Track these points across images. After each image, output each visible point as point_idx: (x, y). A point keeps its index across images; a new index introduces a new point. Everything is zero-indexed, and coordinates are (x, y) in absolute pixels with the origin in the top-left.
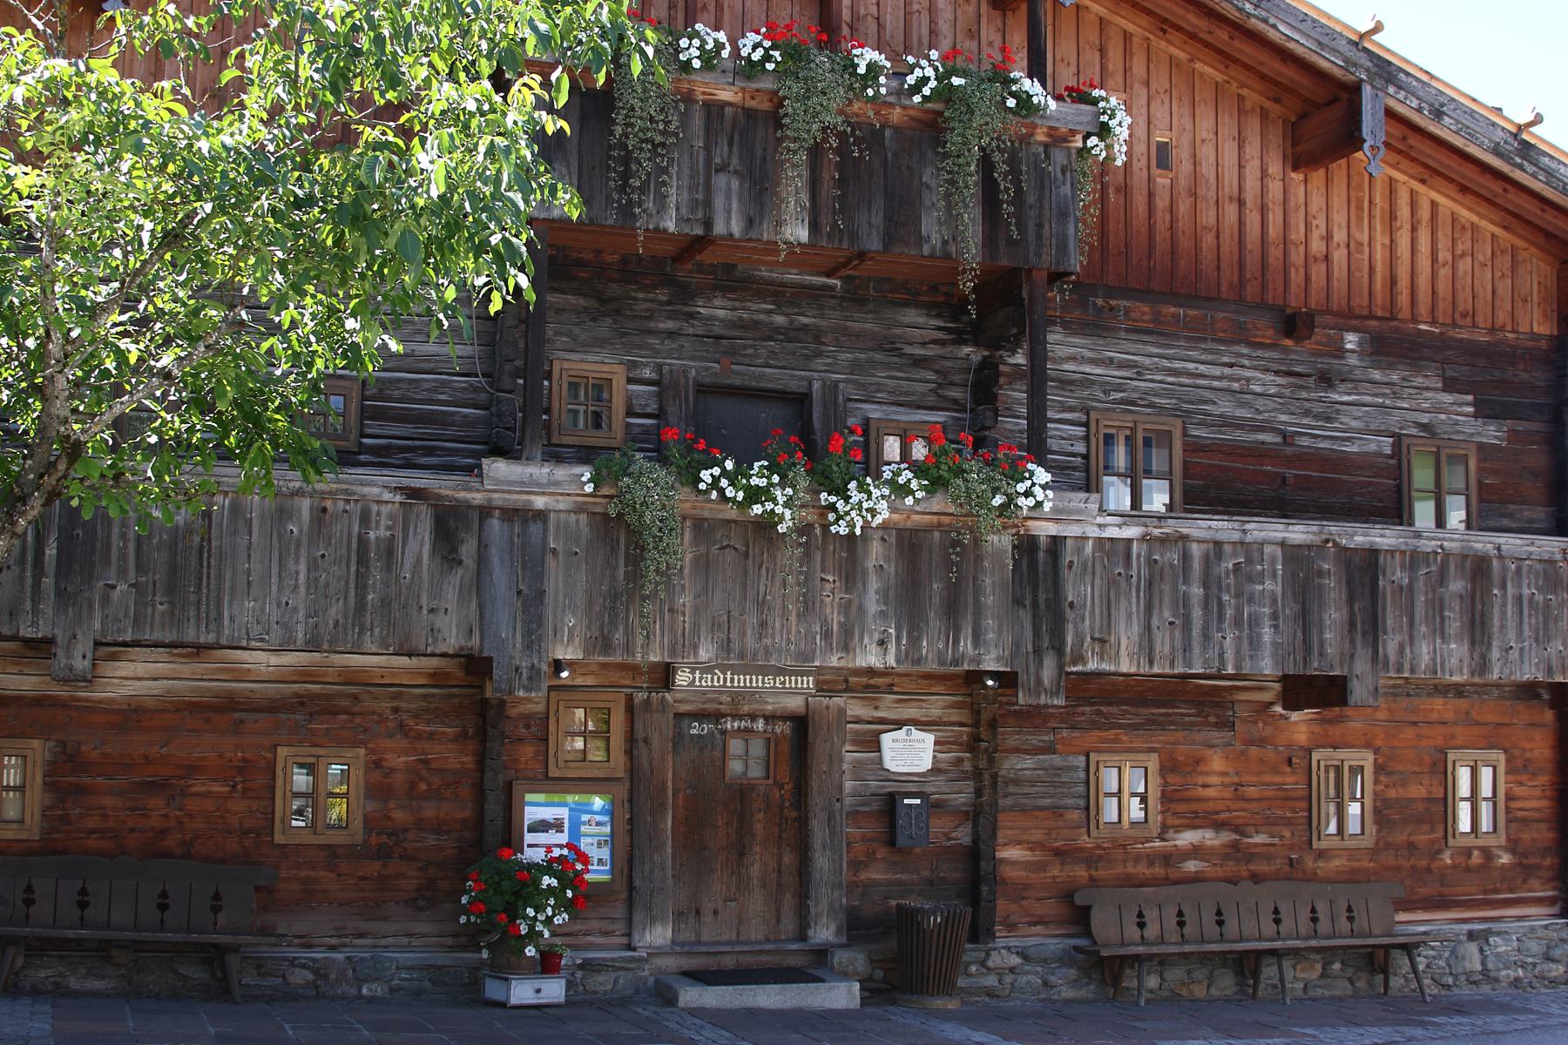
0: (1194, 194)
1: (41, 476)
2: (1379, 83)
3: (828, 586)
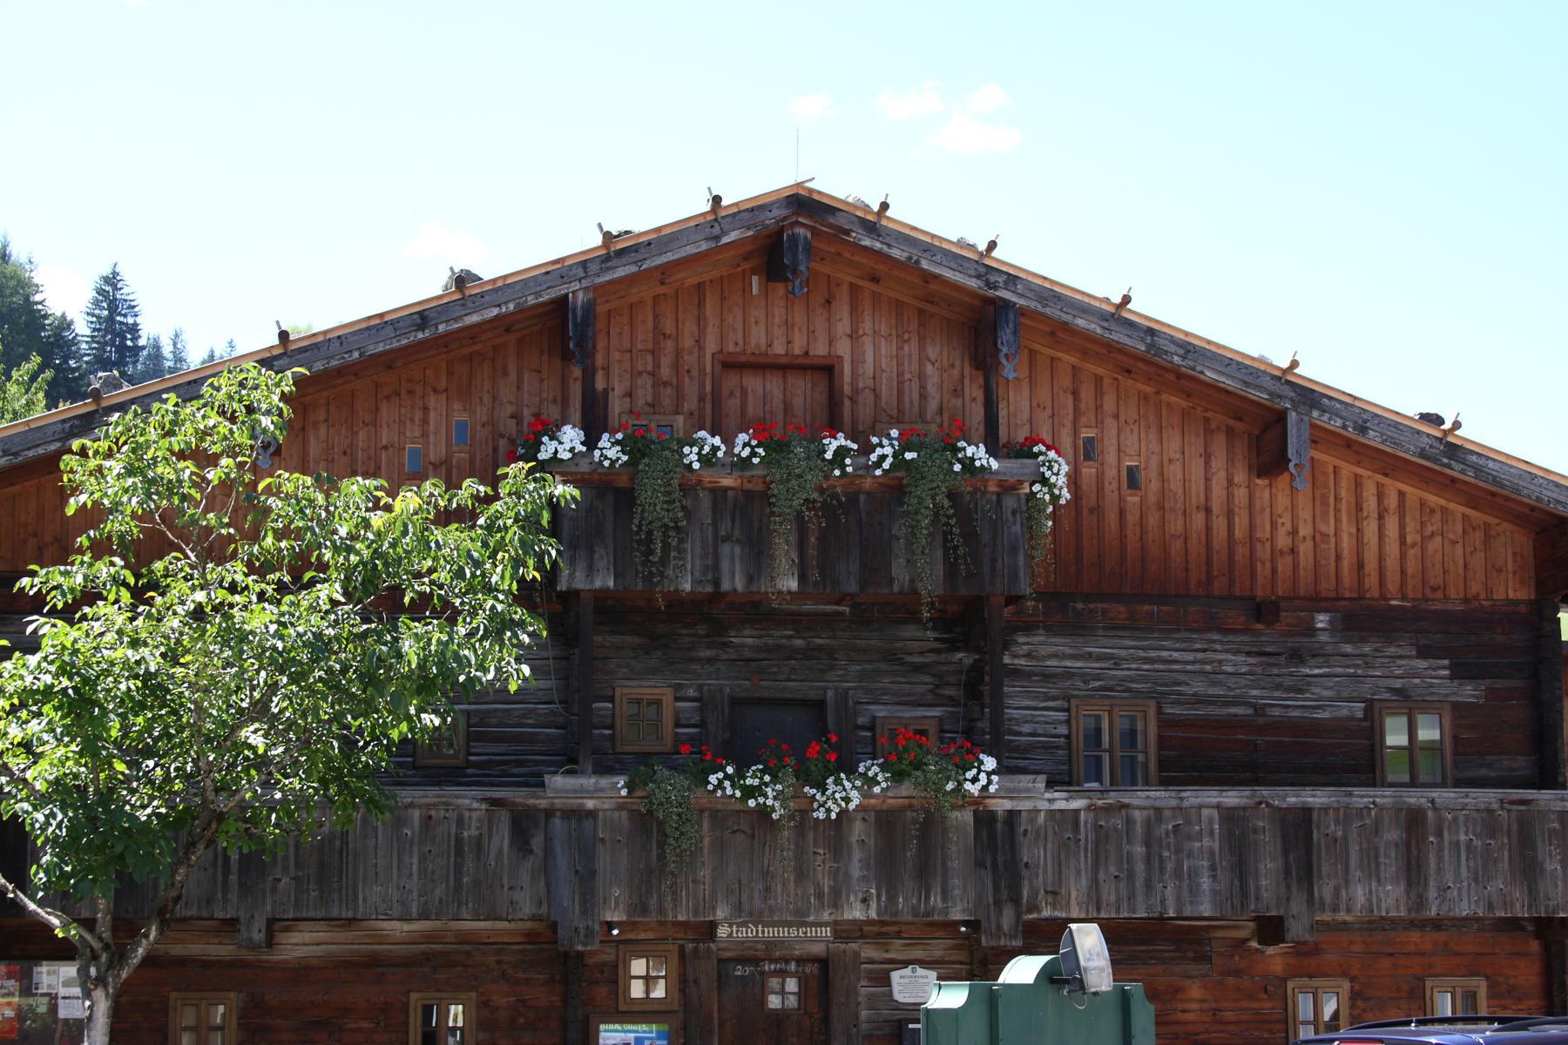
0: (1161, 507)
2: (1302, 409)
3: (819, 858)
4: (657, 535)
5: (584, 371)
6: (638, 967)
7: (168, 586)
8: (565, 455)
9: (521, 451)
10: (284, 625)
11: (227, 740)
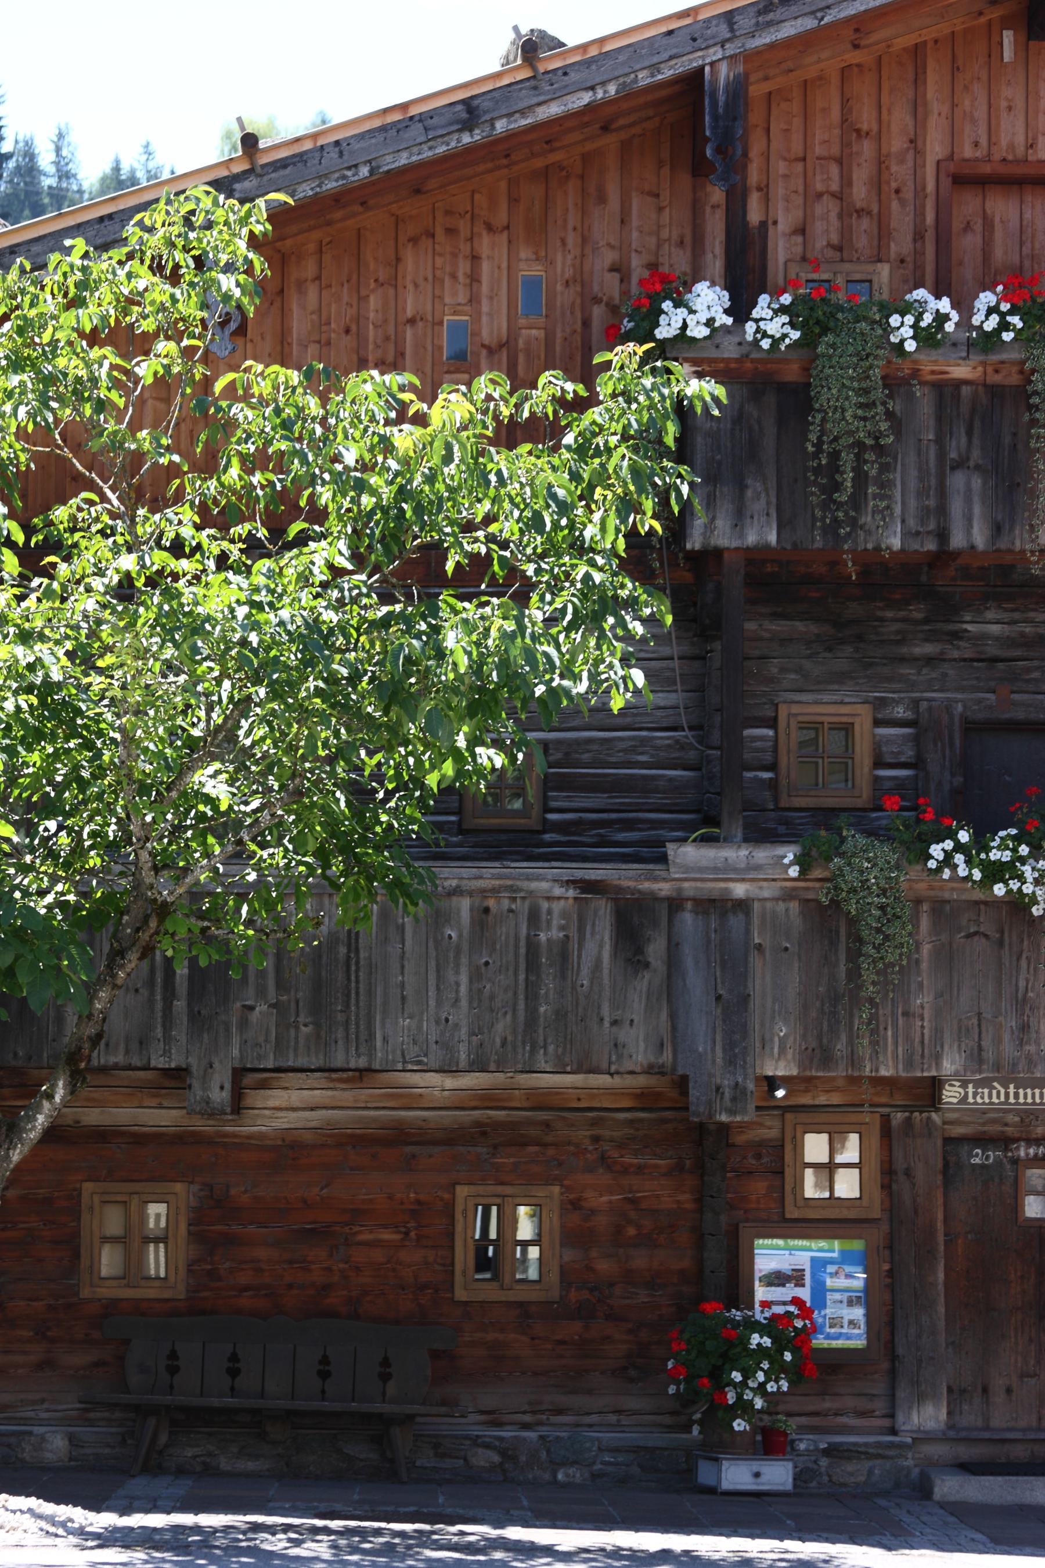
1: (138, 930)
4: (847, 459)
5: (729, 194)
6: (815, 1147)
7: (75, 545)
8: (699, 332)
9: (627, 325)
10: (259, 606)
11: (171, 788)
